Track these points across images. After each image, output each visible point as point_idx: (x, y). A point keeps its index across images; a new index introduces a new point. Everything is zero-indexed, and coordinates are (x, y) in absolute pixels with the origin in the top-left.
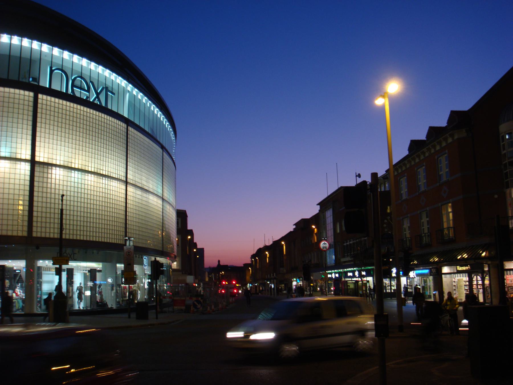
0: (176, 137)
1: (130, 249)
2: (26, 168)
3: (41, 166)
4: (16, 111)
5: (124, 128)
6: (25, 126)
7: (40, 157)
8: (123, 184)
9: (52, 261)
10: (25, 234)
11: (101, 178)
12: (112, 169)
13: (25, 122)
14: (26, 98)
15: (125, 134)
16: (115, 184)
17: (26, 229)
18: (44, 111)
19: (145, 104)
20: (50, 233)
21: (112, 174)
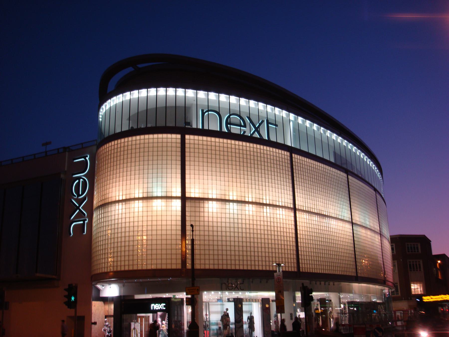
0: (382, 174)
1: (279, 275)
2: (177, 204)
3: (196, 201)
4: (165, 153)
5: (345, 177)
6: (174, 166)
7: (192, 192)
8: (290, 211)
9: (203, 293)
10: (179, 267)
11: (314, 216)
12: (322, 207)
13: (174, 162)
14: (174, 141)
15: (347, 183)
16: (281, 212)
17: (179, 261)
18: (192, 150)
19: (355, 153)
20: (251, 265)
21: (311, 209)
